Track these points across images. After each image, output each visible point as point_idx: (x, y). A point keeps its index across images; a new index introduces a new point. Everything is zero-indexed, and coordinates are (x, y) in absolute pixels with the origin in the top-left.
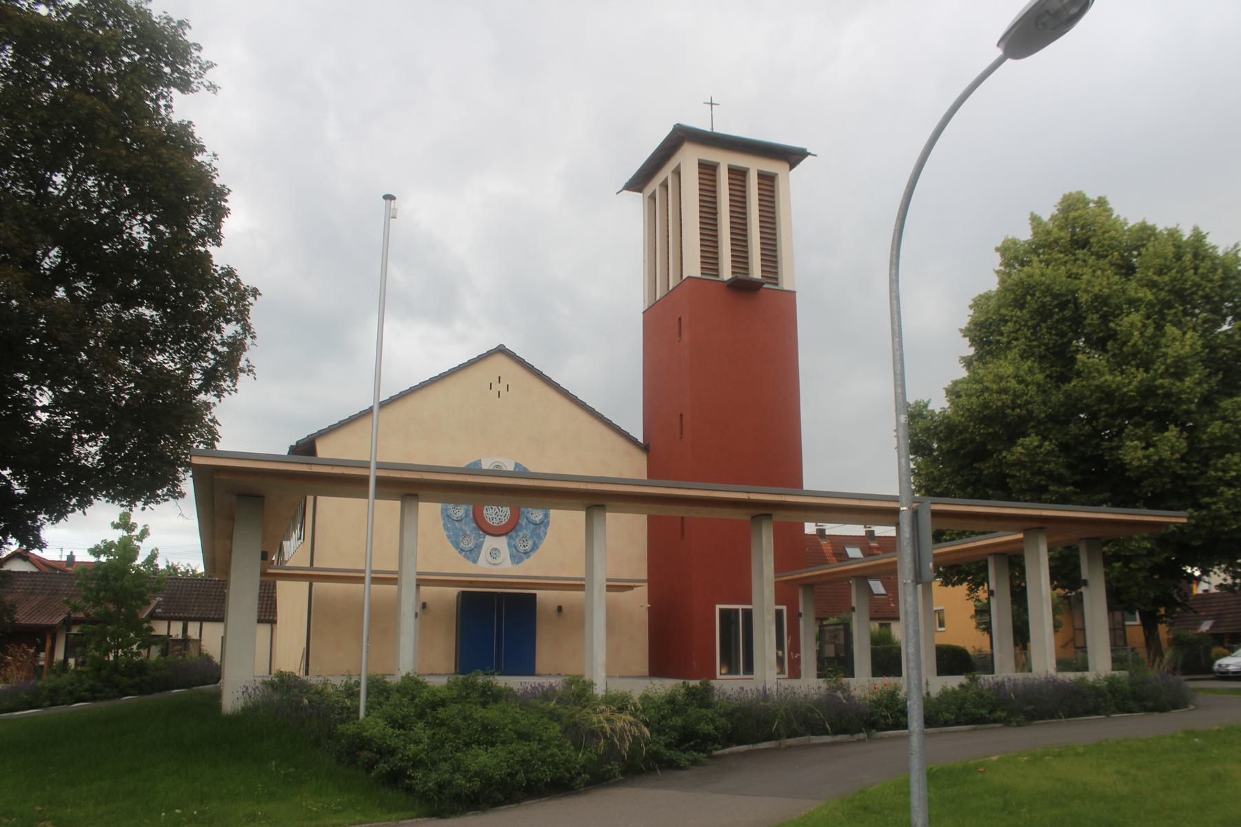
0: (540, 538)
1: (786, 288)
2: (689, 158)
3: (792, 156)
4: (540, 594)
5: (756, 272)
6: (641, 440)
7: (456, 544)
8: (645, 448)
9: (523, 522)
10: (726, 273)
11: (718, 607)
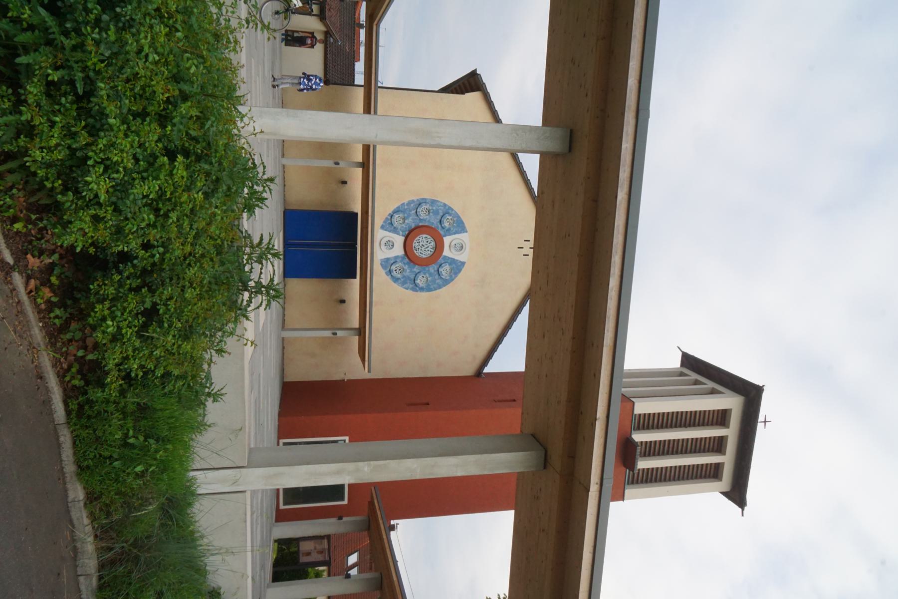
0: (403, 284)
1: (626, 491)
2: (731, 402)
3: (737, 494)
4: (356, 282)
5: (643, 464)
6: (487, 370)
7: (396, 211)
8: (479, 373)
9: (416, 269)
10: (639, 437)
11: (346, 502)
